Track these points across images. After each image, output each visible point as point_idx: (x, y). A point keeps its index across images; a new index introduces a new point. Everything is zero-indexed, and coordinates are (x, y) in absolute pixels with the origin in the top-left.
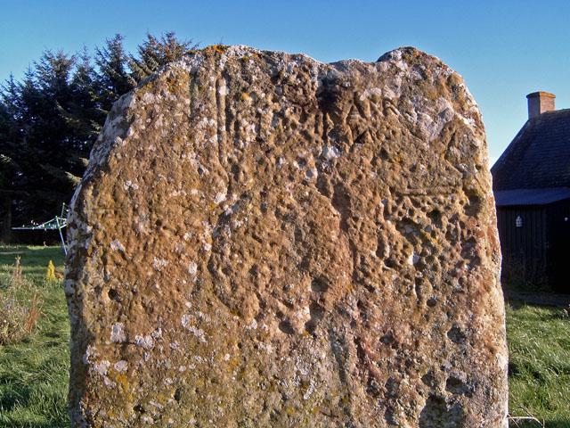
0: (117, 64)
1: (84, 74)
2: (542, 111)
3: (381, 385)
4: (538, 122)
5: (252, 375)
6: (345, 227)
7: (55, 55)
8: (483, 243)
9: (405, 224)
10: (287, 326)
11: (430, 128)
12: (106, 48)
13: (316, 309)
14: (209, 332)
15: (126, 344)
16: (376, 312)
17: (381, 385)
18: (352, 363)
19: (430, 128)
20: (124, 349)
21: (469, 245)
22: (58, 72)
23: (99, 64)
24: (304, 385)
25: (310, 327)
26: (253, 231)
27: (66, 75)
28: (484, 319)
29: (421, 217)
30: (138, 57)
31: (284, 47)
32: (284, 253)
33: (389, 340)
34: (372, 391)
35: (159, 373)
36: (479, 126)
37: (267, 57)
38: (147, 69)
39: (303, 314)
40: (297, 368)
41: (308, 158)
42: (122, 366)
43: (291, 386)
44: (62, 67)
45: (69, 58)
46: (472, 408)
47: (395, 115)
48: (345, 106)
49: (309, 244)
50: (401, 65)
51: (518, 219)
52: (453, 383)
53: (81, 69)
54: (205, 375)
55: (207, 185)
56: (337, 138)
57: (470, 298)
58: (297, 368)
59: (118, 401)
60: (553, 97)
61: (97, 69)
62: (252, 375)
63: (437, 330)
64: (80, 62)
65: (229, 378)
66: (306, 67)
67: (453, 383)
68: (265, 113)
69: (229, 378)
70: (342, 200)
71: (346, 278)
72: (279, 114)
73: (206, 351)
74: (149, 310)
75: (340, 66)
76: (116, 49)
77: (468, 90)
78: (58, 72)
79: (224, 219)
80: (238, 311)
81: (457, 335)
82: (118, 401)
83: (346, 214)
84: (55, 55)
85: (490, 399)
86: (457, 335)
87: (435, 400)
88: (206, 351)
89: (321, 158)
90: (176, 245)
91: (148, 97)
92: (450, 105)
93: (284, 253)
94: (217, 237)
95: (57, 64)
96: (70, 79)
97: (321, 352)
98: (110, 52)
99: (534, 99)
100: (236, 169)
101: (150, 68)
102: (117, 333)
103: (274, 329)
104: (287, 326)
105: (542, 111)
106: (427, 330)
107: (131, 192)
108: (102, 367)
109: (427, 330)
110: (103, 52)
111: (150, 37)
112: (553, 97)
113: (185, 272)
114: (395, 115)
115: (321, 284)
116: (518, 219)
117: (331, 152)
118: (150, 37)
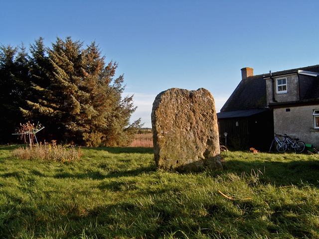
0: (41, 52)
1: (22, 56)
2: (248, 76)
3: (200, 138)
4: (246, 81)
5: (182, 137)
6: (194, 115)
7: (6, 46)
8: (214, 117)
9: (203, 115)
10: (187, 130)
11: (206, 100)
12: (35, 44)
13: (191, 127)
14: (176, 131)
15: (163, 133)
16: (199, 127)
17: (200, 138)
18: (196, 135)
19: (206, 100)
20: (163, 134)
21: (212, 117)
22: (8, 56)
23: (32, 52)
24: (190, 138)
25: (190, 130)
26: (181, 116)
27: (12, 58)
28: (215, 128)
29: (205, 113)
30: (52, 48)
31: (184, 88)
32: (186, 119)
33: (201, 131)
34: (199, 139)
35: (168, 138)
36: (213, 100)
37: (181, 90)
38: (58, 55)
39: (189, 128)
40: (188, 136)
41: (188, 106)
42: (163, 137)
43: (188, 138)
44: (10, 53)
45: (13, 49)
46: (214, 141)
47: (201, 98)
48: (194, 97)
49: (189, 118)
50: (202, 91)
51: (237, 123)
52: (211, 137)
53: (21, 55)
54: (175, 137)
55: (174, 109)
56: (193, 102)
57: (212, 125)
58: (188, 136)
59: (163, 142)
60: (252, 70)
61: (31, 55)
62: (182, 137)
63: (208, 130)
64: (20, 51)
65: (179, 138)
66: (187, 91)
67: (211, 137)
68: (181, 98)
69: (179, 138)
70: (194, 111)
71: (195, 123)
72: (184, 99)
73: (175, 134)
74: (166, 128)
75: (192, 91)
76: (40, 45)
77: (211, 94)
78: (8, 56)
79: (176, 115)
80: (179, 128)
81: (211, 130)
82: (163, 142)
83: (194, 113)
84: (6, 46)
85: (216, 139)
86: (211, 130)
87: (208, 140)
88: (175, 134)
89: (190, 105)
90: (170, 119)
91: (164, 96)
92: (209, 97)
93: (186, 119)
94: (176, 117)
95: (7, 52)
96: (14, 60)
97: (192, 133)
98: (37, 46)
99: (244, 71)
100: (178, 107)
101: (59, 55)
102: (162, 132)
103: (185, 130)
104: (187, 130)
105: (248, 76)
106: (207, 130)
107: (162, 111)
108: (160, 137)
109: (207, 130)
110: (33, 46)
111: (58, 39)
112: (252, 70)
113: (171, 123)
114: (201, 98)
115: (191, 124)
116: (237, 123)
117: (192, 104)
118: (58, 39)
